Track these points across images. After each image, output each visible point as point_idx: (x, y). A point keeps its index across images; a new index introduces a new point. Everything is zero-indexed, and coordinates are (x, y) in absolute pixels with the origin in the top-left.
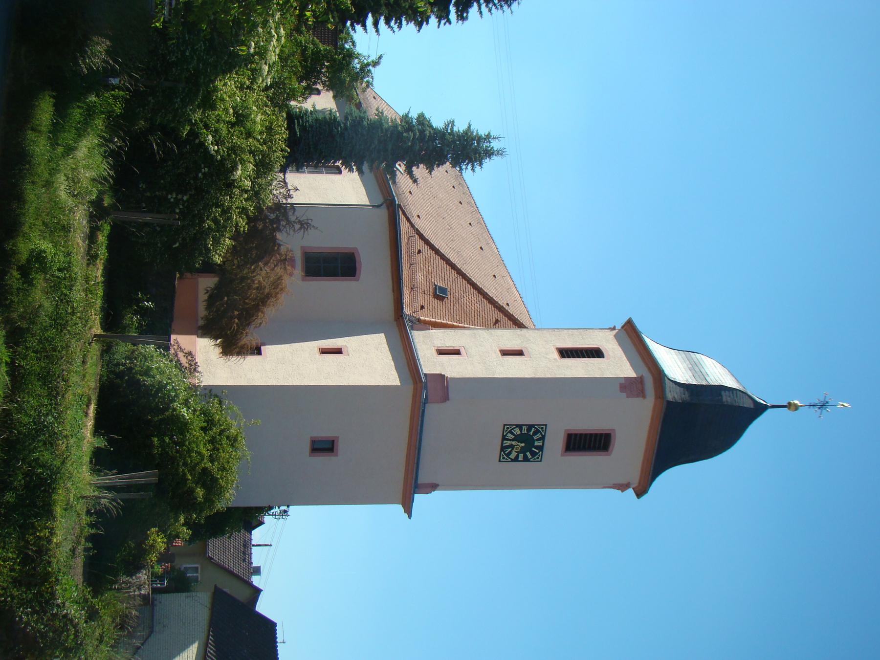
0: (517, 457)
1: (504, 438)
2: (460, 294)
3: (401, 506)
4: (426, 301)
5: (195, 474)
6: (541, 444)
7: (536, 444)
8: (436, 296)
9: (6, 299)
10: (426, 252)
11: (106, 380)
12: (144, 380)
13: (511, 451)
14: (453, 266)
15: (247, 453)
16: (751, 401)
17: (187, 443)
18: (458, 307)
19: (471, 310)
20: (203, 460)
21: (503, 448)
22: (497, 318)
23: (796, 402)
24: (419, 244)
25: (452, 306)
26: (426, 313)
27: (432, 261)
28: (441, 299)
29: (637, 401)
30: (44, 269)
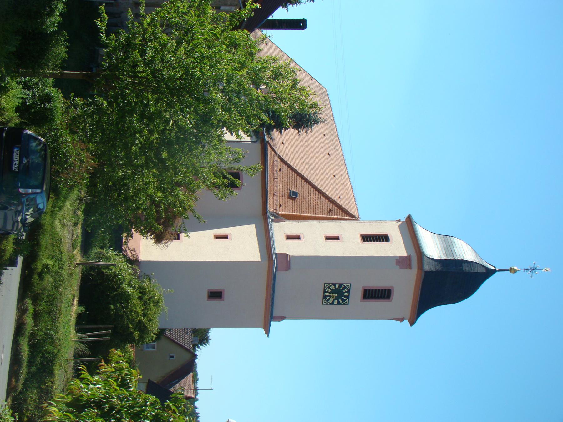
0: (333, 302)
1: (325, 291)
2: (306, 195)
3: (263, 329)
4: (283, 201)
5: (134, 324)
6: (348, 295)
7: (345, 294)
8: (290, 198)
9: (32, 289)
10: (285, 169)
11: (85, 271)
12: (106, 272)
13: (329, 299)
14: (302, 177)
15: (165, 308)
16: (484, 268)
17: (130, 307)
18: (304, 203)
19: (313, 204)
20: (138, 316)
21: (324, 297)
22: (330, 208)
23: (515, 268)
24: (279, 164)
25: (301, 203)
26: (283, 209)
27: (288, 175)
28: (294, 199)
29: (407, 271)
30: (49, 271)
